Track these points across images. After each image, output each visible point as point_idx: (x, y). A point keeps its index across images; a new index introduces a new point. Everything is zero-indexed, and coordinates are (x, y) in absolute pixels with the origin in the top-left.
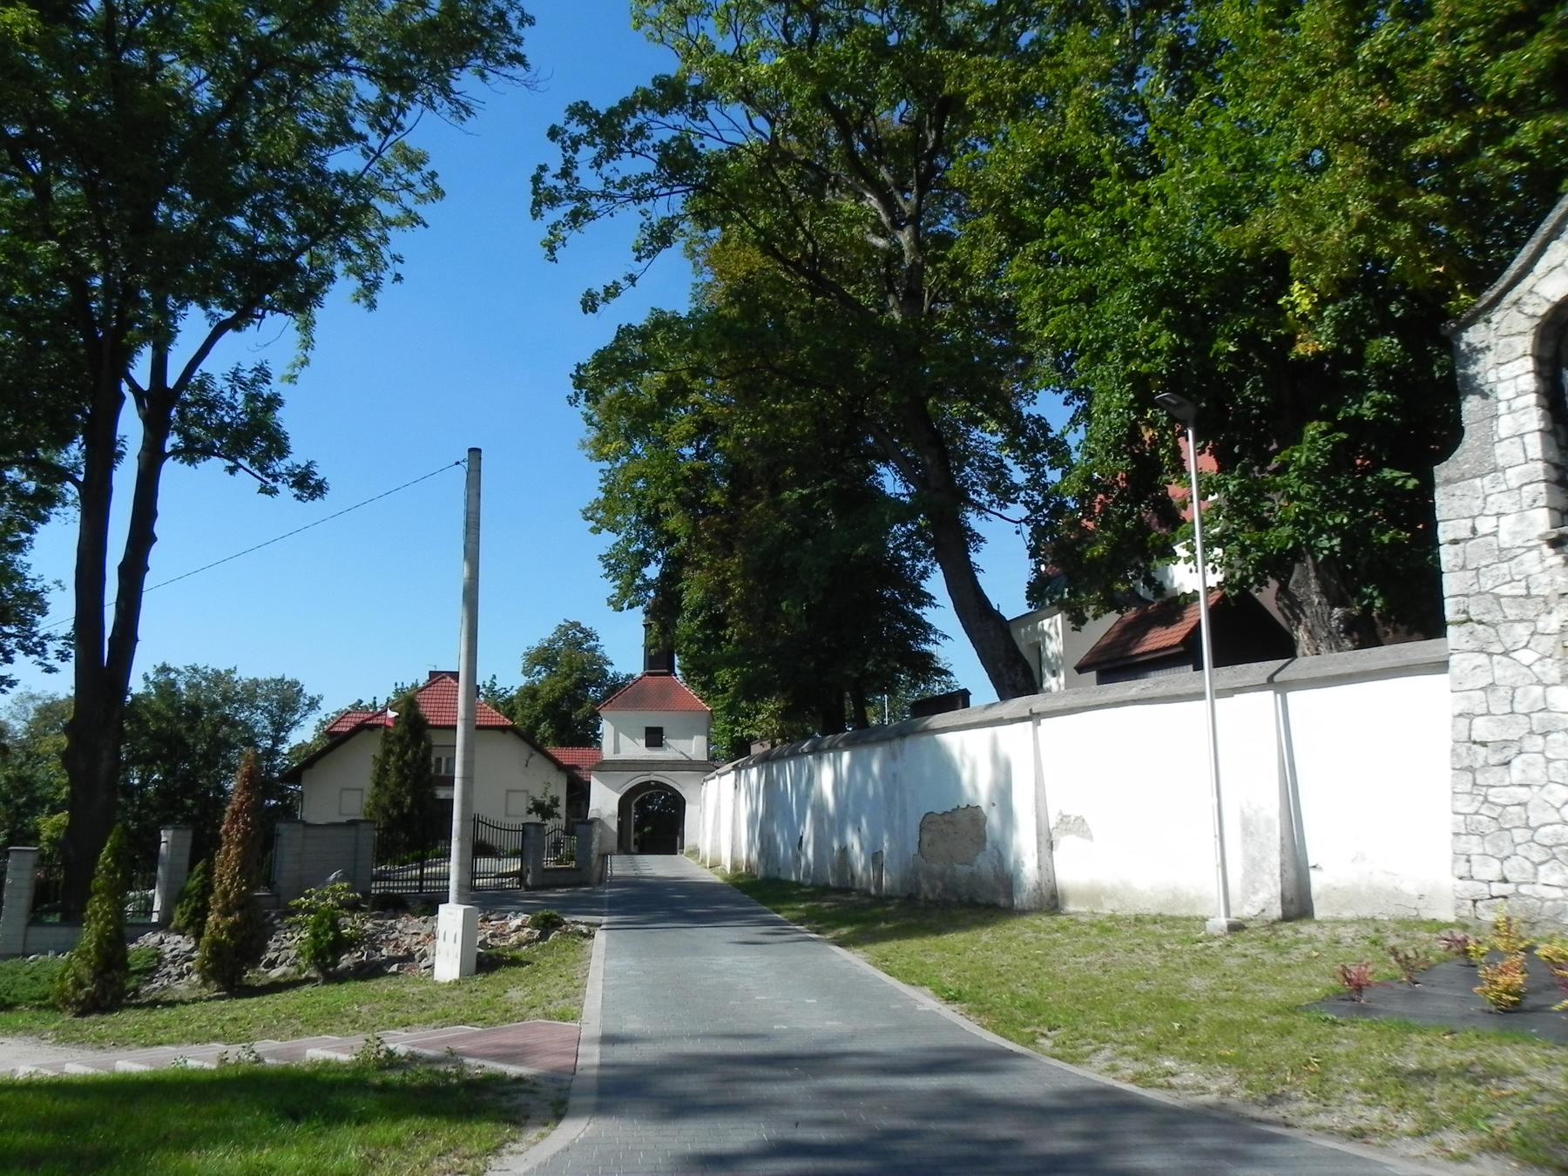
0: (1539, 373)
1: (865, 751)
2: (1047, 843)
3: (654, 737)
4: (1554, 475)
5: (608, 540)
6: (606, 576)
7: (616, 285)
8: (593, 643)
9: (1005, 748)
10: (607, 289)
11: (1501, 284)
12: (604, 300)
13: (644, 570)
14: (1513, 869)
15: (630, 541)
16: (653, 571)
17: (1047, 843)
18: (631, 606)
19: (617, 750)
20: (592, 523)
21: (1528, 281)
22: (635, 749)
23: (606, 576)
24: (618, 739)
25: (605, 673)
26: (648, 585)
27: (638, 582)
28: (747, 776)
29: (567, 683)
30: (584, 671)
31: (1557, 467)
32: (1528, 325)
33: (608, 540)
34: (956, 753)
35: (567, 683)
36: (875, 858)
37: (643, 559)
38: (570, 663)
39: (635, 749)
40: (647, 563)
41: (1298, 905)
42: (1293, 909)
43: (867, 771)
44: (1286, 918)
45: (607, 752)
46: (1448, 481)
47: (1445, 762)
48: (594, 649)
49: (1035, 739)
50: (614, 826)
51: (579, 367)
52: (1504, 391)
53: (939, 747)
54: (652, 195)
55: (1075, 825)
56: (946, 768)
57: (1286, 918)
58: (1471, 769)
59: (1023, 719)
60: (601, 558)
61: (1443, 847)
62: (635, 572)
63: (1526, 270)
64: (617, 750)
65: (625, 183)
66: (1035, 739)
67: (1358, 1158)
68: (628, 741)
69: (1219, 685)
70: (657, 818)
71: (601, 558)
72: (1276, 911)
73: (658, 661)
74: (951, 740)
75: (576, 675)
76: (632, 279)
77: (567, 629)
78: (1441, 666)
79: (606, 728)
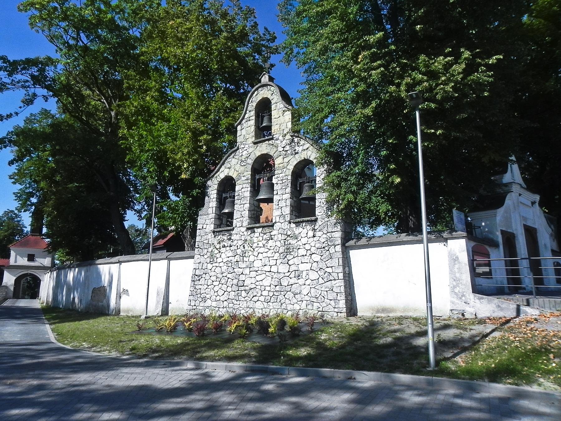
0: (217, 194)
1: (81, 268)
2: (119, 296)
3: (31, 258)
4: (217, 217)
5: (18, 187)
6: (16, 200)
7: (11, 114)
8: (19, 219)
9: (112, 271)
10: (7, 116)
11: (214, 172)
12: (6, 119)
13: (31, 199)
14: (197, 303)
15: (26, 188)
16: (34, 200)
17: (119, 296)
18: (25, 211)
19: (16, 262)
20: (13, 180)
21: (219, 173)
22: (23, 261)
23: (16, 200)
24: (16, 258)
25: (23, 231)
26: (33, 204)
27: (29, 203)
28: (75, 270)
29: (6, 233)
30: (14, 229)
31: (218, 215)
32: (217, 183)
33: (18, 187)
34: (101, 270)
35: (6, 233)
36: (80, 301)
37: (31, 195)
38: (8, 226)
39: (23, 261)
40: (33, 197)
41: (165, 312)
42: (164, 313)
43: (81, 274)
44: (162, 315)
45: (12, 261)
46: (201, 215)
47: (190, 279)
48: (19, 221)
49: (119, 268)
50: (12, 289)
51: (31, 115)
52: (212, 197)
53: (97, 268)
54: (29, 87)
55: (126, 292)
56: (99, 276)
57: (162, 315)
58: (194, 281)
59: (117, 263)
60: (14, 193)
61: (187, 297)
62: (28, 199)
63: (218, 170)
64: (16, 262)
65: (18, 82)
66: (119, 268)
67: (18, 354)
68: (21, 258)
69: (152, 258)
70: (29, 285)
71: (14, 193)
72: (160, 314)
73: (36, 229)
74: (100, 267)
75: (10, 231)
76: (17, 114)
77: (9, 213)
78: (193, 257)
79: (13, 254)
